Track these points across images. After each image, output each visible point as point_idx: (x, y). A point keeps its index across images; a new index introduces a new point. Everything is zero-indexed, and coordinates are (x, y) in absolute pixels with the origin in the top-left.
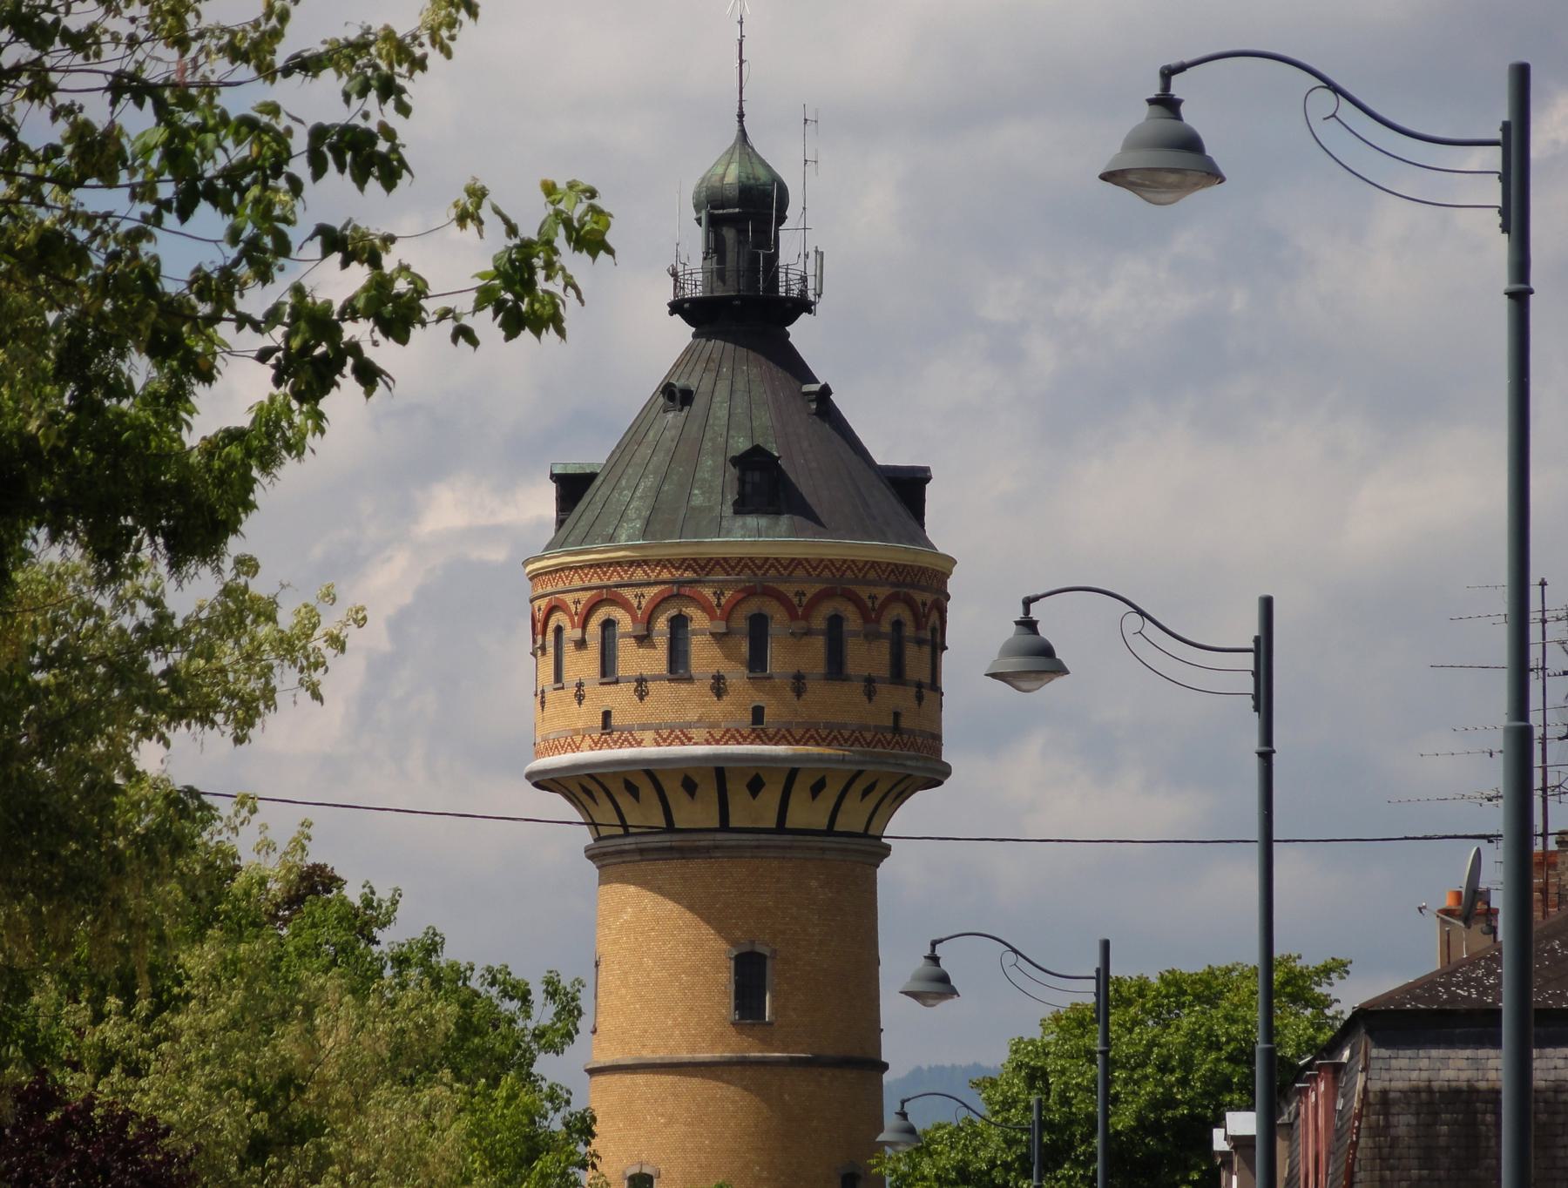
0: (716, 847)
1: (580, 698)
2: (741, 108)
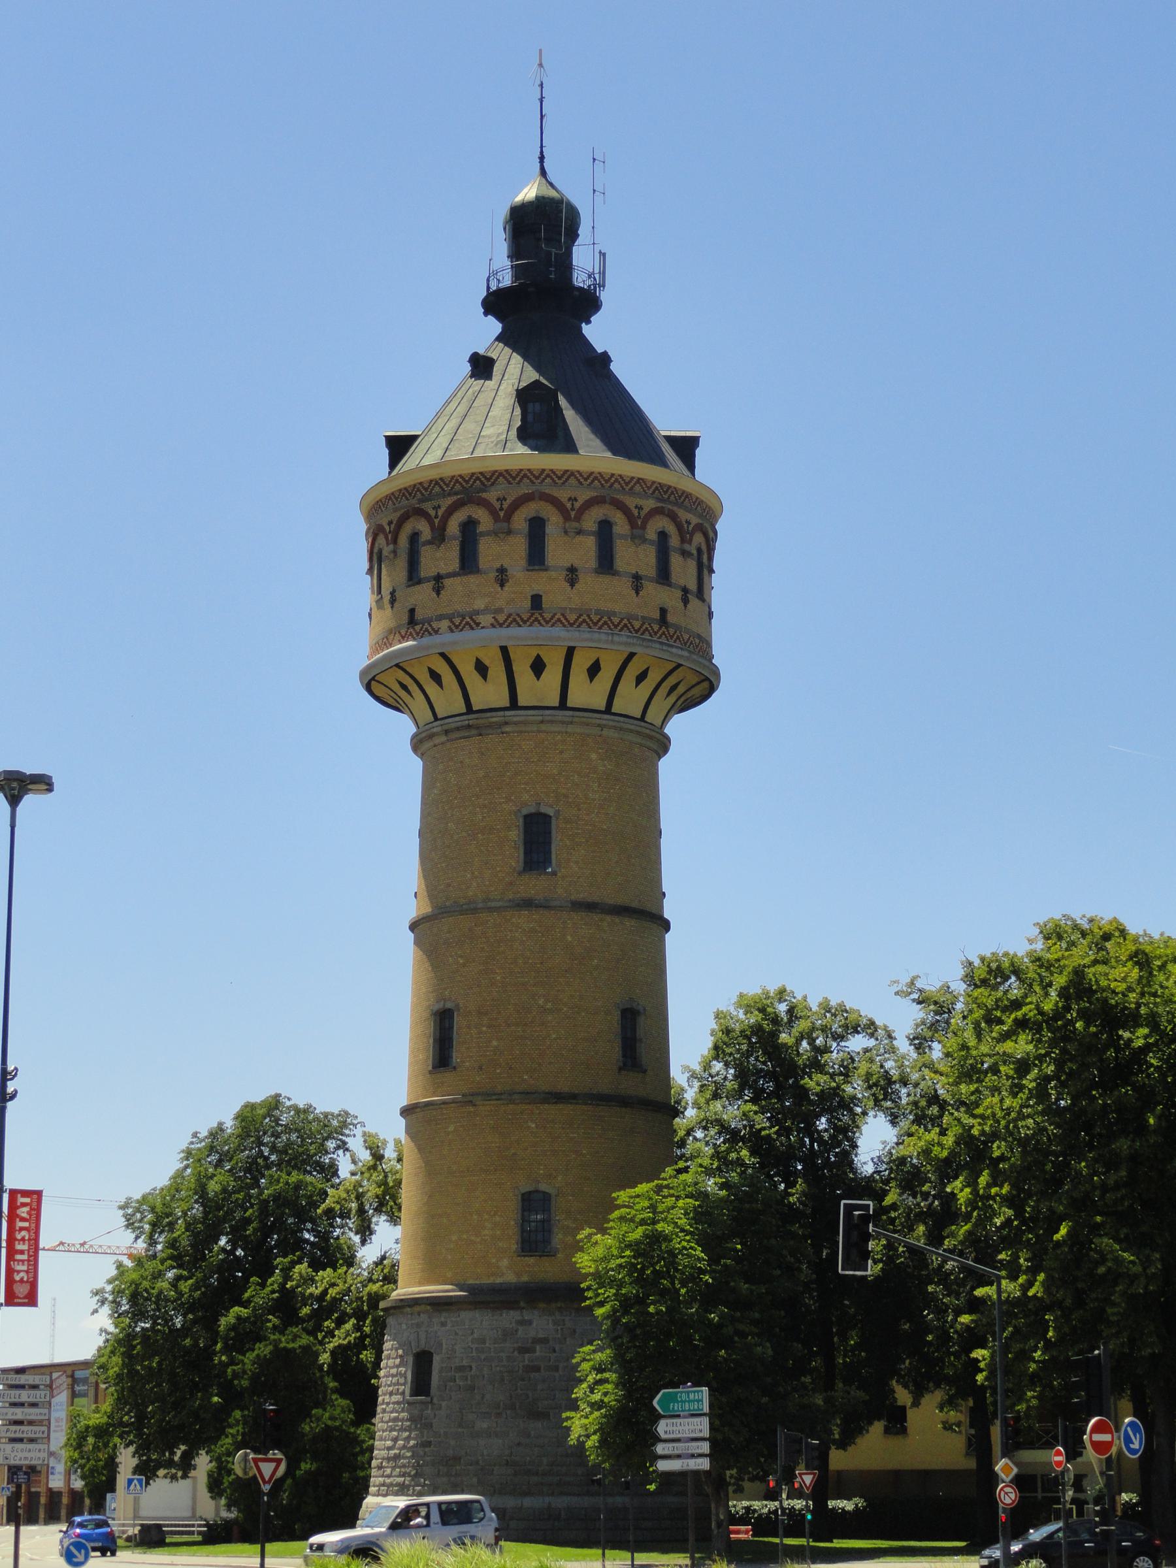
2: (542, 152)
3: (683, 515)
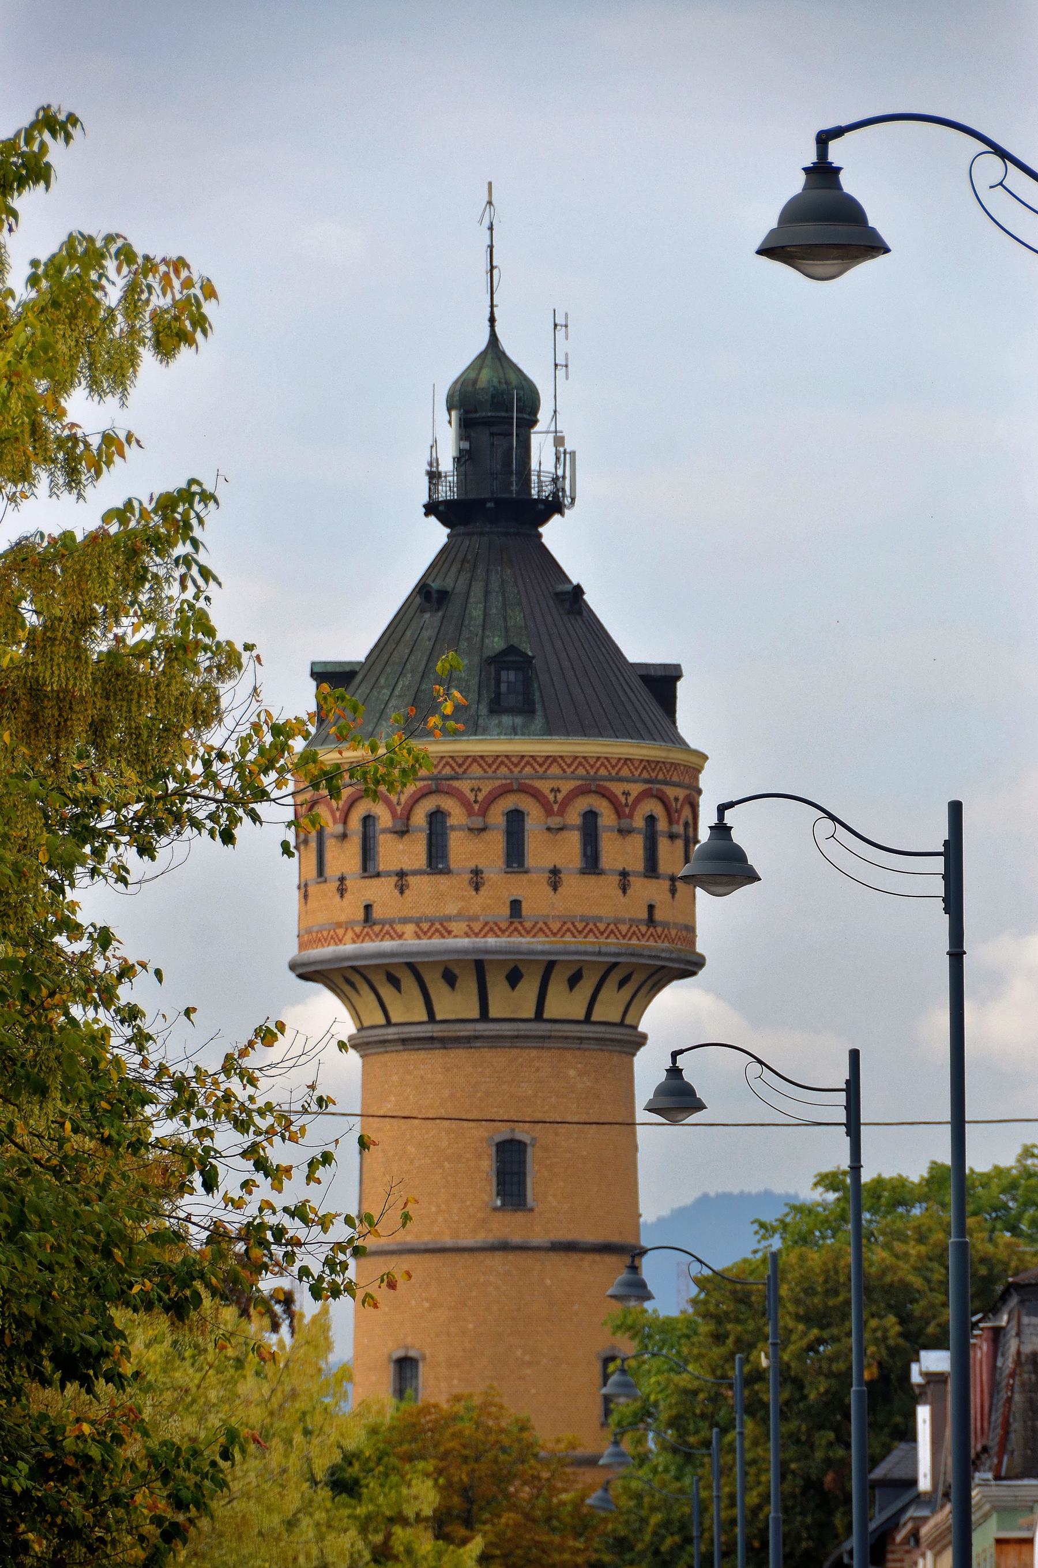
0: (476, 1038)
1: (342, 891)
2: (492, 313)
3: (671, 792)
